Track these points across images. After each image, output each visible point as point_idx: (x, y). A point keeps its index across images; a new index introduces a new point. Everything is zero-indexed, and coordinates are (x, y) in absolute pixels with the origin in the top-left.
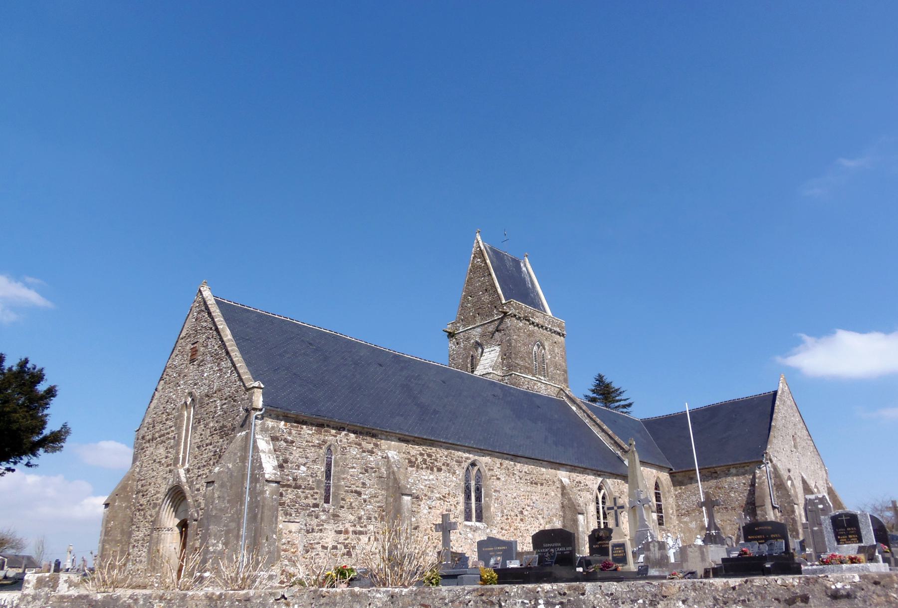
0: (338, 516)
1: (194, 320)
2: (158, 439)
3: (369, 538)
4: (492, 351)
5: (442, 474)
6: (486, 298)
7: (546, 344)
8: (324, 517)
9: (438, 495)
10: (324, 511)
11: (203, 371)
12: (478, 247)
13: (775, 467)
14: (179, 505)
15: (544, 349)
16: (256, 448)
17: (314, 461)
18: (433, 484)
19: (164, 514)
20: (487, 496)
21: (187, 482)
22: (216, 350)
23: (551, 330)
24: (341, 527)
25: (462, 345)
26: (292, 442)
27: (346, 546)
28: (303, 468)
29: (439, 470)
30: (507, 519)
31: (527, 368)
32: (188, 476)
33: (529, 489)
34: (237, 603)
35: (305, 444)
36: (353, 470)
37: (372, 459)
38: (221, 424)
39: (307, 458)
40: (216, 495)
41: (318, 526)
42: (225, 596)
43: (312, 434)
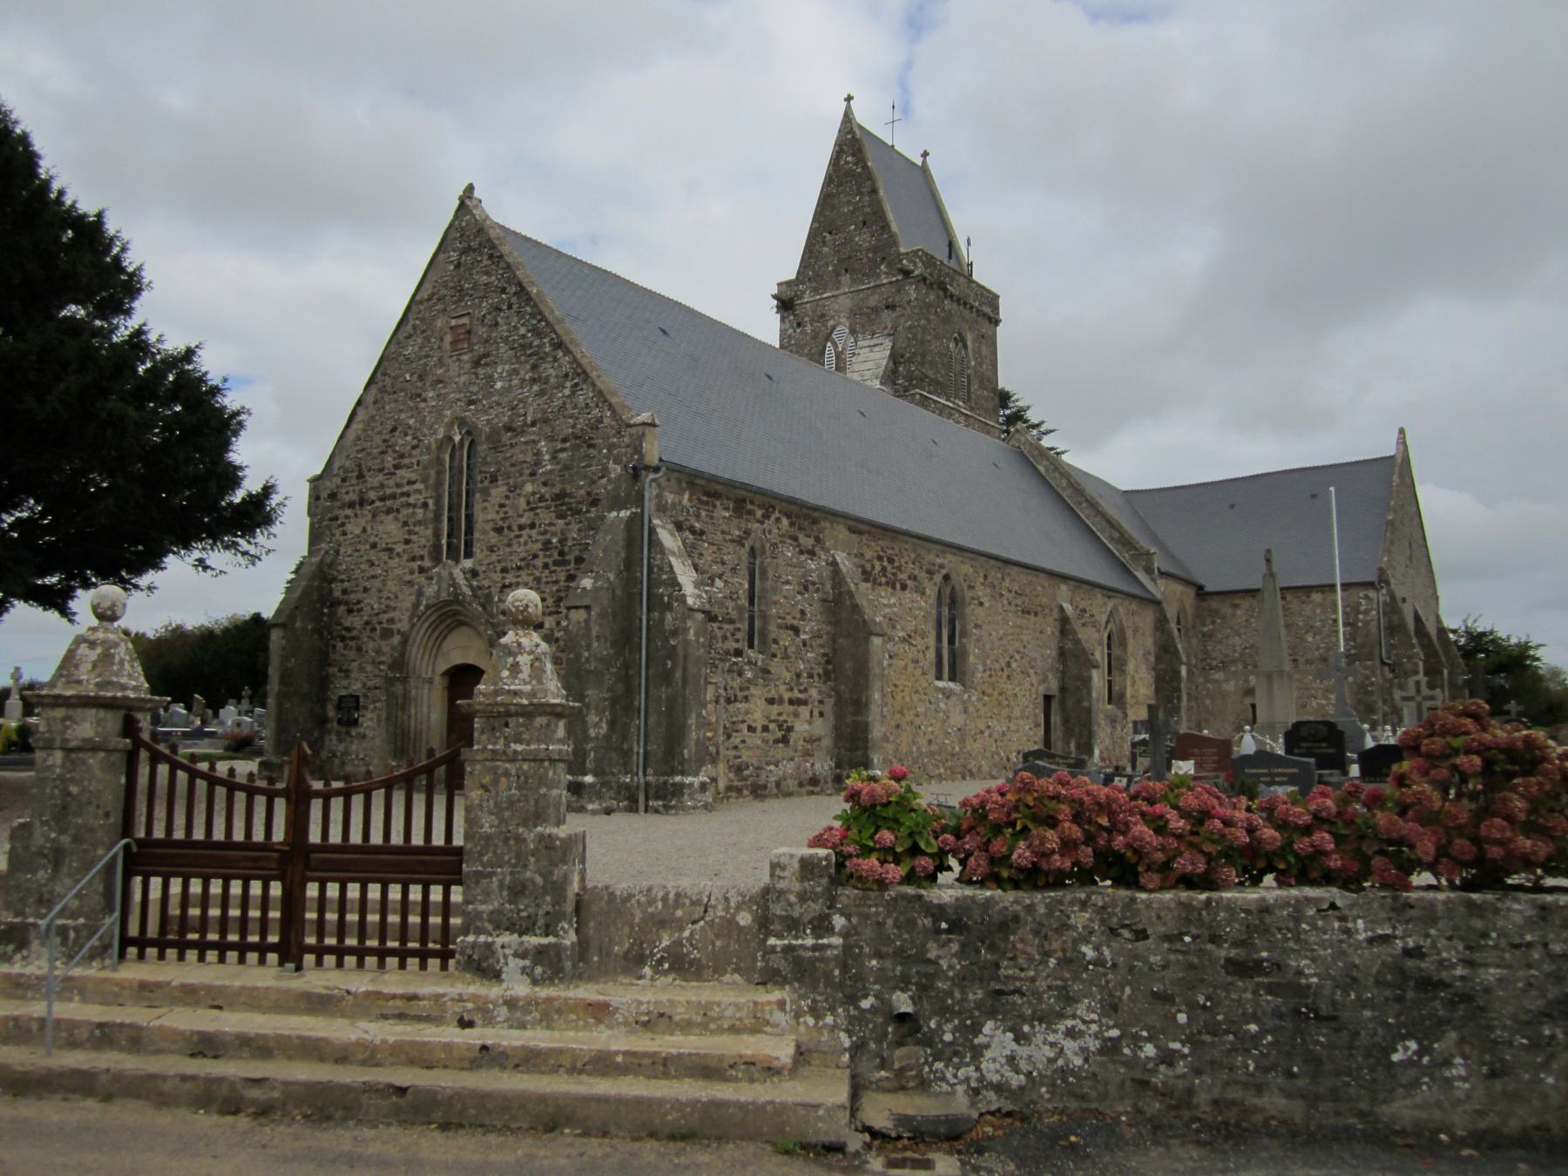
0: (769, 672)
1: (452, 267)
2: (378, 504)
3: (812, 712)
4: (875, 345)
5: (907, 594)
6: (864, 239)
7: (969, 338)
8: (749, 675)
9: (901, 634)
10: (750, 663)
11: (491, 377)
12: (849, 133)
13: (1392, 595)
14: (445, 638)
15: (965, 347)
16: (655, 543)
17: (734, 570)
18: (895, 613)
19: (414, 651)
20: (964, 634)
21: (475, 596)
22: (524, 336)
23: (978, 311)
24: (773, 692)
25: (809, 329)
26: (702, 533)
27: (780, 727)
28: (719, 583)
29: (904, 587)
30: (991, 676)
31: (938, 383)
32: (475, 583)
33: (1019, 621)
34: (1243, 915)
35: (720, 536)
36: (788, 587)
37: (813, 567)
38: (557, 490)
39: (723, 563)
40: (594, 633)
41: (741, 689)
42: (1217, 903)
43: (728, 518)
